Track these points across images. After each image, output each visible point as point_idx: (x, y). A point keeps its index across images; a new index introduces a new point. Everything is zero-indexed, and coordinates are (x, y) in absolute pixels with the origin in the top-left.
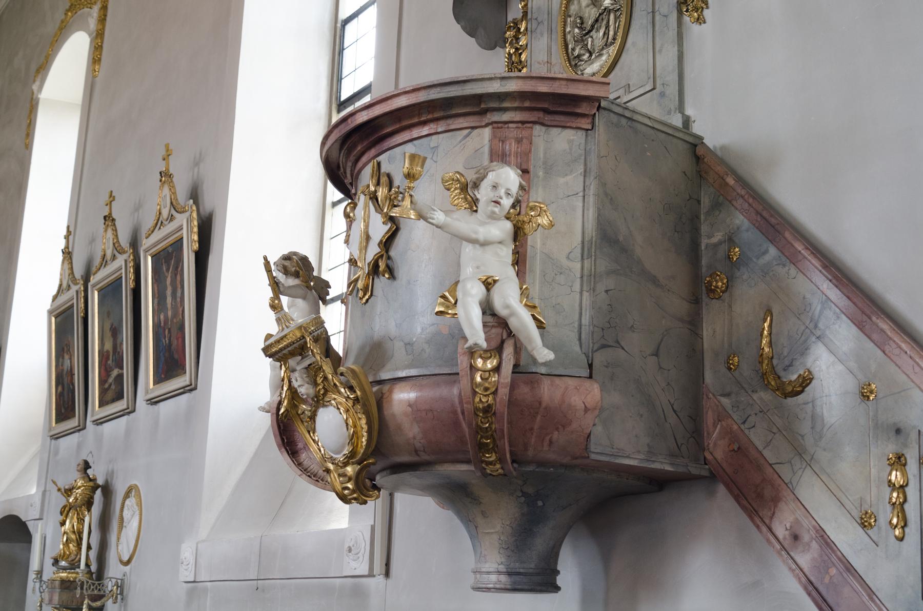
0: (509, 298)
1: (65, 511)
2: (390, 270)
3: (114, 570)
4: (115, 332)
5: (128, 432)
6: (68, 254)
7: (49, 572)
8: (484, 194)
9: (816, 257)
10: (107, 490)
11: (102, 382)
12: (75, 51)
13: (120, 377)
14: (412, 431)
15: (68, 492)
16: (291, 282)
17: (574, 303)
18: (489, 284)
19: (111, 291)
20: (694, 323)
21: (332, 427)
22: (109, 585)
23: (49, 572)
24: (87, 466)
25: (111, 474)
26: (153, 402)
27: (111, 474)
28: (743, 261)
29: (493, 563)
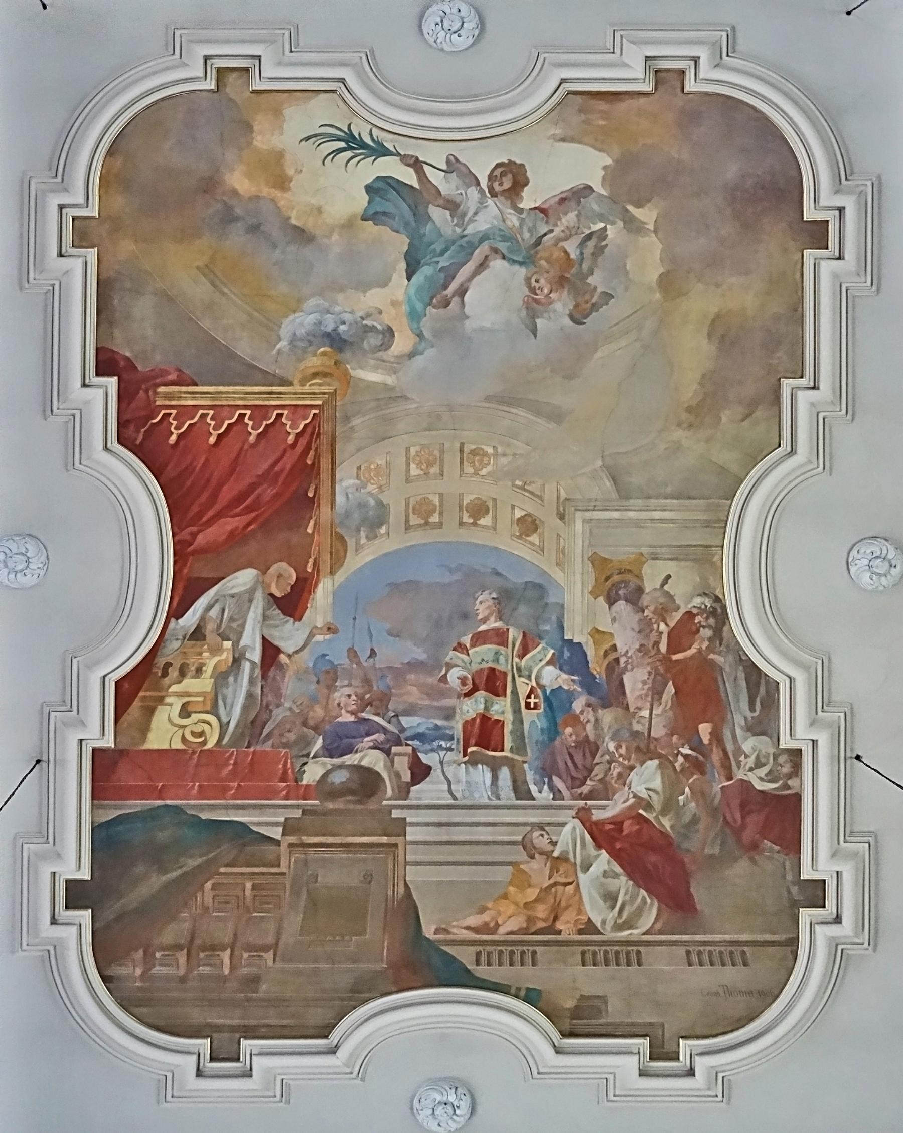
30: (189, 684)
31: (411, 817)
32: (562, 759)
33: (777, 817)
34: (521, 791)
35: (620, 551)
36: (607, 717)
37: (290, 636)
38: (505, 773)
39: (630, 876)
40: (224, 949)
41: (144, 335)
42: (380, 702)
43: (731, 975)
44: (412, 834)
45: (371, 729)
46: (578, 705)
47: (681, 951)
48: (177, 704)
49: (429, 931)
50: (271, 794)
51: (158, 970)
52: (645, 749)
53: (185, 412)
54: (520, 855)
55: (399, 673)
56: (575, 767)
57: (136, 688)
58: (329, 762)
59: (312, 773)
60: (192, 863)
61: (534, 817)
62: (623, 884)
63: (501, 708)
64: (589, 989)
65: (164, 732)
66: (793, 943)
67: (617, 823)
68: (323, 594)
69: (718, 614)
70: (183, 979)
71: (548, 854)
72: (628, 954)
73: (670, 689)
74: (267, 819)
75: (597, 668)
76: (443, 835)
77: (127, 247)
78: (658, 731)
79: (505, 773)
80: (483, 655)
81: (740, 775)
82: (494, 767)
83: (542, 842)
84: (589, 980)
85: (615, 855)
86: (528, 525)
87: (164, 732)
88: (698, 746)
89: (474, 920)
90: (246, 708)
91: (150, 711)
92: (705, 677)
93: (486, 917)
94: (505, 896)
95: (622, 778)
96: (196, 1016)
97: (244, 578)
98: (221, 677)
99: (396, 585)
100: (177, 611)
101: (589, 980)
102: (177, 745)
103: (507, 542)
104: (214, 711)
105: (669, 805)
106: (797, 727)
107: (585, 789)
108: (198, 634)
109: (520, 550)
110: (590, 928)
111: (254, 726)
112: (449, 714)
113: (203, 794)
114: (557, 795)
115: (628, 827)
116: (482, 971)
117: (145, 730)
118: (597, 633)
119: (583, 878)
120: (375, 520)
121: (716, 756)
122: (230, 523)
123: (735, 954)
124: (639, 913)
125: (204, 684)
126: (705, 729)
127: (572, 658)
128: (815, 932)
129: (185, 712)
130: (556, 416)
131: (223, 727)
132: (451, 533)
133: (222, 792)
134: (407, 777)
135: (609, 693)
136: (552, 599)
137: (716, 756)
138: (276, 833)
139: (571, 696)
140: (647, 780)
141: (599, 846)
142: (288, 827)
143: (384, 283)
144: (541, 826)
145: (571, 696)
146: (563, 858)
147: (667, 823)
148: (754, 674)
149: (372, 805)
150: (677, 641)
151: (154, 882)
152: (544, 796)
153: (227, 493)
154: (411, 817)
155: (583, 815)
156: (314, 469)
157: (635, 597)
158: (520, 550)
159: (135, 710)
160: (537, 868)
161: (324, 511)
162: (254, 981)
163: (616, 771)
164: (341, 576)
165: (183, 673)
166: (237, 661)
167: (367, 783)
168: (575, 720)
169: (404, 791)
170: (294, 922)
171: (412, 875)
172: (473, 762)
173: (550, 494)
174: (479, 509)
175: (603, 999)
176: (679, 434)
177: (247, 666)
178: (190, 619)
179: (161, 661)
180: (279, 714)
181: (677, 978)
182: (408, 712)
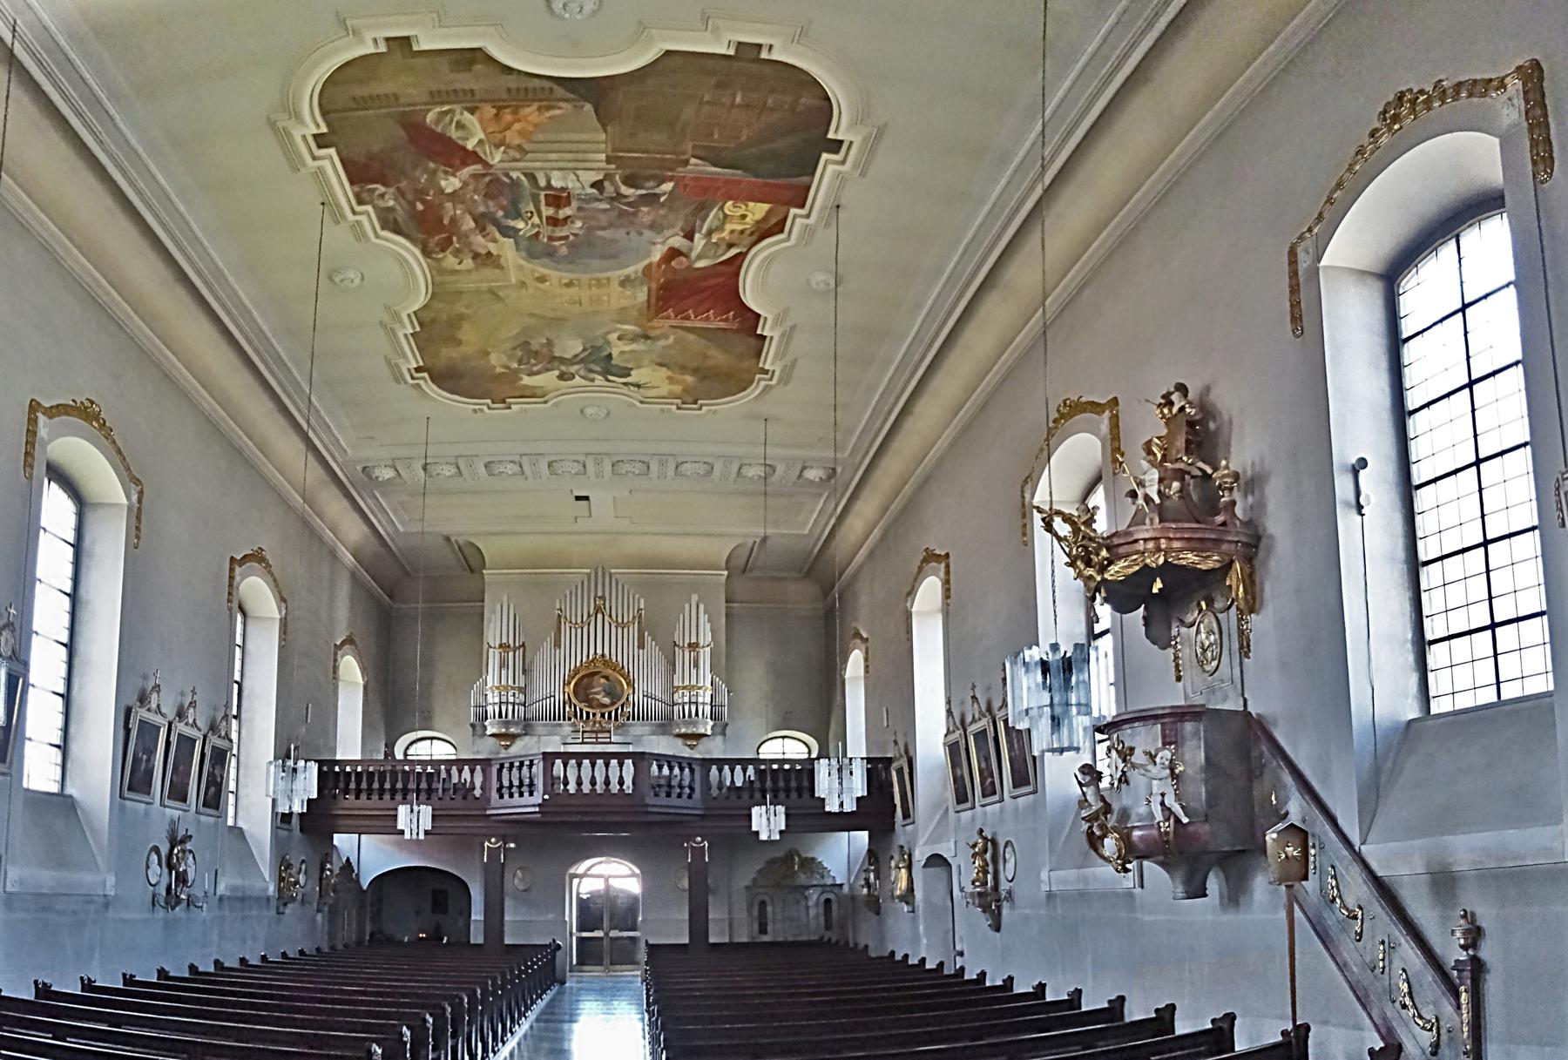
0: (1170, 801)
1: (974, 856)
2: (1127, 782)
3: (1004, 886)
4: (987, 759)
5: (1001, 811)
6: (949, 712)
7: (969, 889)
8: (1158, 760)
9: (1070, 1045)
10: (994, 842)
11: (982, 784)
12: (930, 590)
13: (993, 783)
14: (1141, 846)
15: (974, 846)
16: (1088, 778)
17: (1199, 792)
18: (1163, 795)
19: (981, 736)
20: (1250, 789)
21: (1110, 845)
22: (1004, 894)
23: (969, 889)
24: (981, 831)
25: (994, 834)
26: (1015, 798)
27: (994, 834)
28: (1264, 766)
29: (1180, 889)
30: (739, 227)
31: (603, 165)
32: (507, 190)
33: (360, 173)
34: (532, 177)
35: (488, 273)
36: (482, 209)
37: (678, 241)
38: (543, 183)
39: (450, 139)
40: (739, 106)
41: (743, 344)
42: (622, 214)
43: (360, 91)
44: (603, 157)
45: (629, 204)
46: (501, 213)
47: (402, 100)
48: (748, 220)
49: (588, 107)
50: (695, 179)
51: (789, 99)
52: (453, 196)
53: (726, 320)
54: (527, 147)
55: (611, 225)
56: (495, 186)
57: (770, 228)
58: (657, 191)
59: (668, 186)
60: (754, 150)
61: (521, 164)
62: (454, 134)
63: (548, 211)
64: (461, 76)
65: (758, 210)
66: (324, 113)
67: (465, 164)
68: (657, 255)
69: (426, 253)
70: (772, 91)
71: (508, 147)
72: (437, 98)
73: (446, 222)
74: (697, 166)
75: (492, 229)
76: (580, 156)
77: (746, 365)
78: (449, 205)
79: (543, 183)
80: (559, 232)
81: (391, 190)
82: (549, 186)
83: (512, 153)
84: (464, 81)
85: (464, 149)
86: (542, 279)
87: (758, 210)
88: (424, 202)
89: (557, 112)
90: (707, 216)
91: (765, 219)
92: (427, 227)
93: (548, 114)
94: (535, 125)
95: (465, 184)
96: (767, 69)
97: (700, 264)
98: (720, 228)
99: (613, 255)
100: (741, 257)
101: (464, 81)
102: (751, 204)
103: (552, 274)
104: (726, 216)
105: (434, 172)
106: (367, 217)
107: (487, 179)
108: (730, 246)
109: (545, 271)
110: (472, 111)
111: (702, 210)
112: (580, 209)
113: (739, 182)
114: (507, 175)
115: (457, 162)
116: (547, 84)
117: (769, 212)
118: (495, 241)
119: (482, 136)
120: (625, 282)
121: (410, 197)
122: (705, 284)
123: (362, 103)
124: (438, 121)
125: (729, 227)
126: (420, 207)
127: (507, 232)
128: (314, 124)
129: (744, 217)
130: (532, 315)
131: (722, 208)
132: (584, 277)
133: (727, 182)
134: (606, 184)
135: (482, 221)
136: (524, 254)
137: (410, 197)
138: (693, 161)
139: (506, 216)
140: (451, 184)
141: (475, 153)
142: (687, 162)
143: (622, 353)
144: (516, 160)
145: (506, 216)
146: (497, 146)
147: (432, 165)
148: (398, 232)
149: (628, 172)
150: (449, 241)
151: (780, 144)
152: (514, 175)
153: (707, 293)
154: (603, 165)
155: (486, 165)
156: (658, 299)
157: (476, 256)
158: (545, 271)
159: (773, 221)
160: (512, 137)
161: (654, 285)
162: (718, 86)
163: (471, 187)
164: (646, 262)
165: (742, 232)
166: (710, 233)
167: (630, 181)
168: (502, 208)
169: (608, 177)
170: (688, 112)
171: (603, 137)
172: (563, 189)
173: (531, 291)
174: (570, 284)
175: (452, 71)
176: (469, 311)
177: (704, 230)
178: (733, 251)
179: (754, 237)
180: (687, 211)
181: (405, 86)
182: (605, 211)
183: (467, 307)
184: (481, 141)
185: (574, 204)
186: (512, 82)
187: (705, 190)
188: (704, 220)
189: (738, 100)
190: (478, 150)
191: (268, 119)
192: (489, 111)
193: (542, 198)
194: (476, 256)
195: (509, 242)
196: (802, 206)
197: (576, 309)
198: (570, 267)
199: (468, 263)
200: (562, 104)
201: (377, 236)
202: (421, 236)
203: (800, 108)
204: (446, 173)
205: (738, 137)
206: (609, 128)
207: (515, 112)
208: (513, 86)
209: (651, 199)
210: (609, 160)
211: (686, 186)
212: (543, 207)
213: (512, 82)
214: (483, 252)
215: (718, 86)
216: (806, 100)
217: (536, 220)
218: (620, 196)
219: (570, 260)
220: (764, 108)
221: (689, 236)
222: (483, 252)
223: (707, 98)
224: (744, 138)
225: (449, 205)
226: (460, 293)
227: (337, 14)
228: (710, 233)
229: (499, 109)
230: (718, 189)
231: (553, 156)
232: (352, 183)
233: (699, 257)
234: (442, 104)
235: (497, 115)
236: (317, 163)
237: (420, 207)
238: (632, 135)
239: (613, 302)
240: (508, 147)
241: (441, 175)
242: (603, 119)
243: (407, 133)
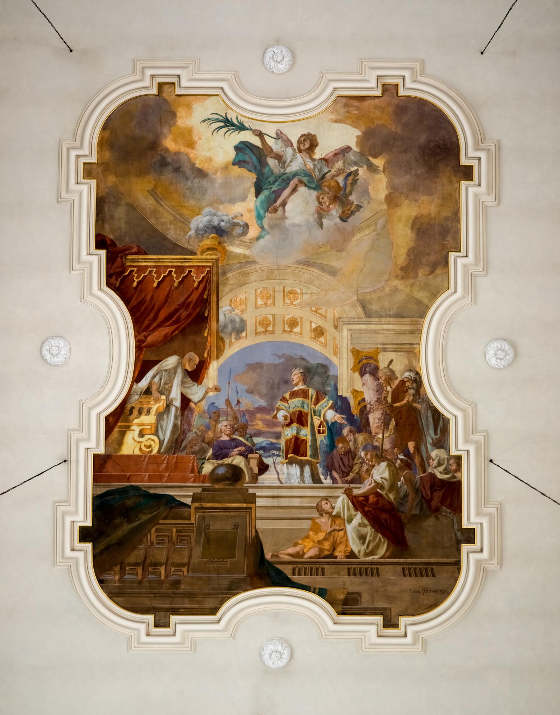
34: (316, 479)
36: (361, 438)
37: (195, 393)
40: (160, 564)
44: (260, 502)
45: (238, 444)
46: (345, 431)
47: (399, 568)
49: (268, 556)
54: (315, 514)
59: (208, 468)
62: (369, 531)
63: (305, 433)
69: (418, 381)
70: (140, 582)
71: (330, 514)
74: (184, 494)
75: (355, 410)
78: (387, 446)
79: (307, 469)
82: (302, 465)
84: (353, 584)
87: (131, 445)
88: (407, 453)
89: (291, 550)
91: (123, 434)
94: (307, 537)
95: (368, 472)
98: (160, 416)
100: (137, 379)
101: (353, 584)
102: (137, 452)
104: (156, 434)
106: (458, 443)
110: (352, 555)
114: (334, 481)
115: (372, 499)
124: (377, 546)
126: (411, 445)
127: (342, 405)
130: (333, 272)
131: (161, 442)
132: (279, 337)
133: (160, 478)
134: (256, 470)
135: (360, 424)
136: (331, 373)
138: (188, 501)
139: (341, 427)
141: (356, 509)
142: (195, 498)
144: (326, 498)
145: (341, 427)
146: (338, 516)
147: (392, 496)
153: (163, 314)
157: (374, 373)
158: (315, 346)
161: (213, 325)
164: (222, 360)
165: (140, 413)
166: (168, 406)
167: (235, 474)
169: (254, 479)
171: (260, 525)
172: (291, 462)
174: (293, 323)
177: (173, 410)
179: (129, 406)
180: (190, 436)
182: (258, 434)
183: (395, 290)
184: (350, 521)
185: (282, 443)
186: (320, 581)
187: (176, 466)
188: (175, 426)
189: (162, 569)
190: (353, 512)
191: (501, 568)
192: (340, 554)
193: (309, 452)
194: (374, 373)
195: (344, 391)
196: (96, 456)
197: (289, 283)
198: (289, 352)
199: (383, 361)
200: (287, 558)
201: (456, 417)
202: (418, 406)
203: (117, 568)
204: (382, 487)
205: (157, 531)
206: (254, 533)
207: (321, 550)
208: (319, 579)
209: (221, 452)
210: (253, 498)
211: (192, 471)
212: (309, 438)
213: (320, 581)
214: (367, 377)
215: (176, 583)
216: (113, 577)
217: (317, 422)
218: (244, 455)
219: (290, 362)
220: (143, 564)
221: (185, 401)
222: (367, 377)
223: (185, 570)
224: (153, 530)
225: (387, 446)
226: (398, 315)
227: (425, 653)
228: (168, 406)
229: (332, 556)
230: (167, 468)
231: (296, 502)
232: (459, 483)
233: (174, 370)
234: (372, 563)
235: (334, 549)
236: (479, 520)
237: (411, 445)
238: (236, 527)
239: (252, 297)
240: (330, 514)
241: (386, 484)
242: (257, 545)
243: (404, 538)
